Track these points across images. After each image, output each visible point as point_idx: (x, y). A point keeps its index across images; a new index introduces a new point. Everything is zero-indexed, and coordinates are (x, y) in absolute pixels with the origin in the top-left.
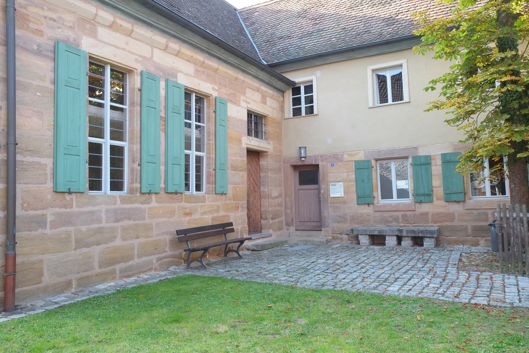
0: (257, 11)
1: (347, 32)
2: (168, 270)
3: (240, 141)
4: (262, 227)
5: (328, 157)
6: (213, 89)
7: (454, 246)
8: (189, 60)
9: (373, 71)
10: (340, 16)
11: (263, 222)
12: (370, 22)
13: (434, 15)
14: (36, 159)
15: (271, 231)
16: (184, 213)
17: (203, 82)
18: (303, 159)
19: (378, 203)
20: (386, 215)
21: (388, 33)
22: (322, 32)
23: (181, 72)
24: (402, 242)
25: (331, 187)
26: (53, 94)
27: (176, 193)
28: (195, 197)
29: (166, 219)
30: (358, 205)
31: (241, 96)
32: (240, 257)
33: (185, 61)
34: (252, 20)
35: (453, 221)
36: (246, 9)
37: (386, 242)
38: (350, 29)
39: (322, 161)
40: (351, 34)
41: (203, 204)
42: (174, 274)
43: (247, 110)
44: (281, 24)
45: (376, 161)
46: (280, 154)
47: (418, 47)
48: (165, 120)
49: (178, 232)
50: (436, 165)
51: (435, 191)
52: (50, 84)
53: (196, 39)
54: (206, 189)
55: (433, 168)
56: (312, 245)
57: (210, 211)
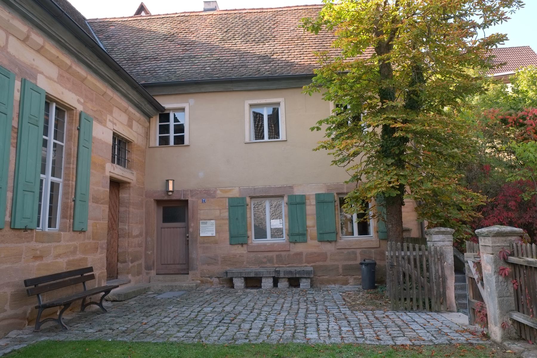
0: (113, 25)
1: (222, 63)
2: (6, 336)
3: (104, 168)
4: (119, 272)
5: (199, 192)
6: (78, 101)
7: (326, 285)
8: (53, 60)
9: (251, 106)
10: (213, 47)
11: (120, 265)
12: (246, 57)
13: (308, 60)
15: (130, 277)
16: (33, 257)
17: (67, 91)
18: (170, 193)
19: (252, 243)
20: (260, 255)
21: (266, 70)
22: (194, 59)
23: (42, 73)
24: (279, 284)
25: (201, 225)
27: (25, 229)
28: (48, 234)
29: (8, 266)
30: (231, 246)
31: (108, 116)
32: (104, 310)
33: (48, 62)
34: (107, 34)
35: (325, 261)
36: (98, 21)
37: (262, 284)
38: (225, 60)
39: (192, 196)
40: (227, 66)
41: (58, 244)
42: (20, 342)
43: (113, 132)
44: (144, 43)
45: (251, 198)
46: (142, 187)
47: (308, 87)
48: (18, 131)
49: (27, 283)
50: (310, 205)
51: (309, 231)
53: (66, 37)
54: (60, 225)
55: (308, 208)
56: (180, 290)
57: (65, 253)
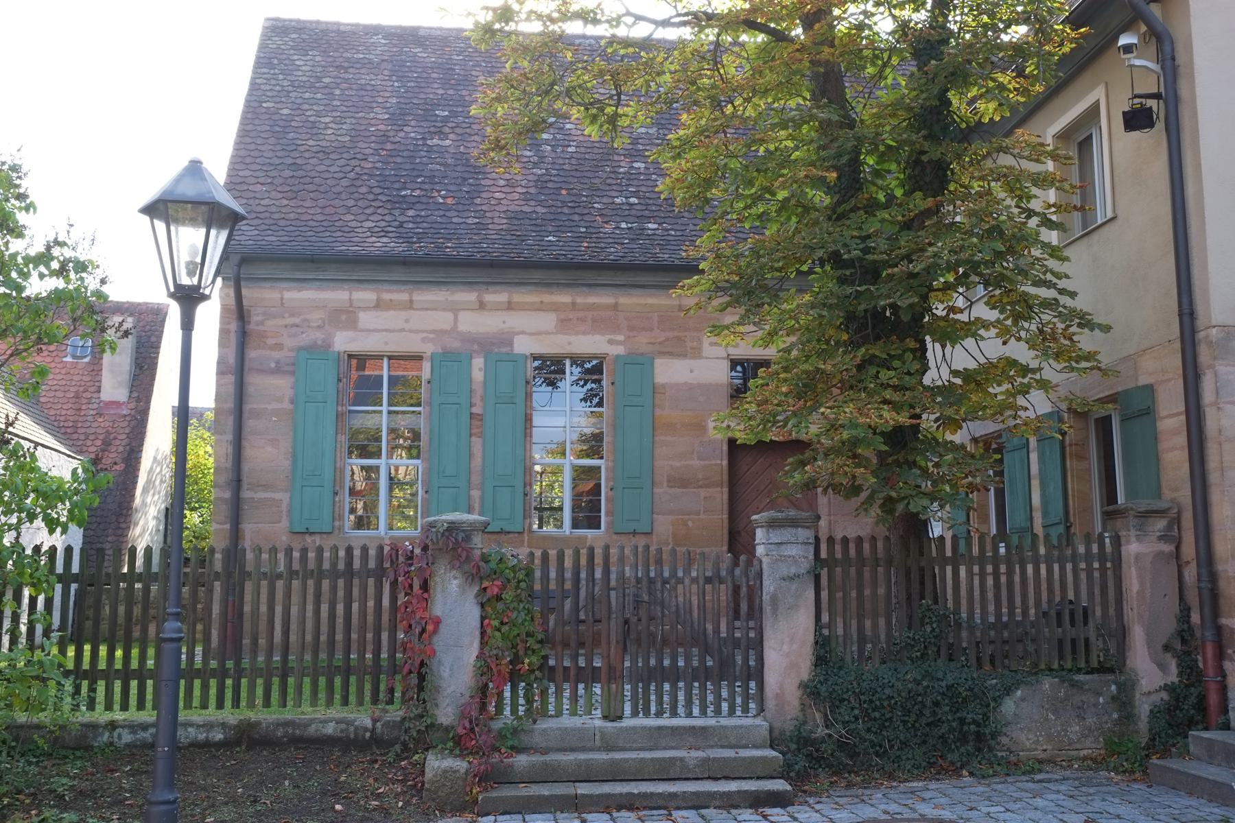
8: (540, 308)
14: (261, 495)
33: (533, 313)
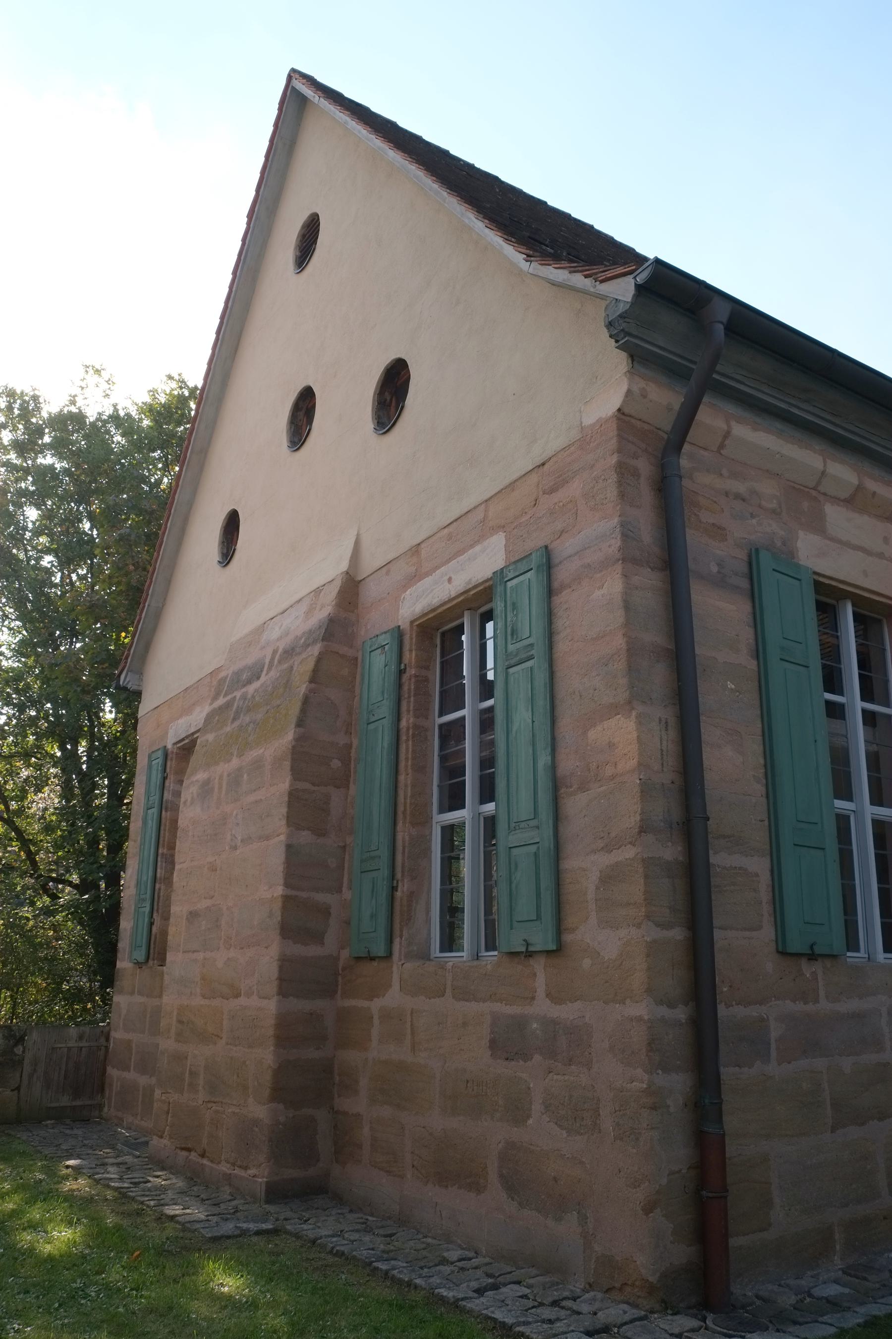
26: (756, 683)
52: (750, 658)
